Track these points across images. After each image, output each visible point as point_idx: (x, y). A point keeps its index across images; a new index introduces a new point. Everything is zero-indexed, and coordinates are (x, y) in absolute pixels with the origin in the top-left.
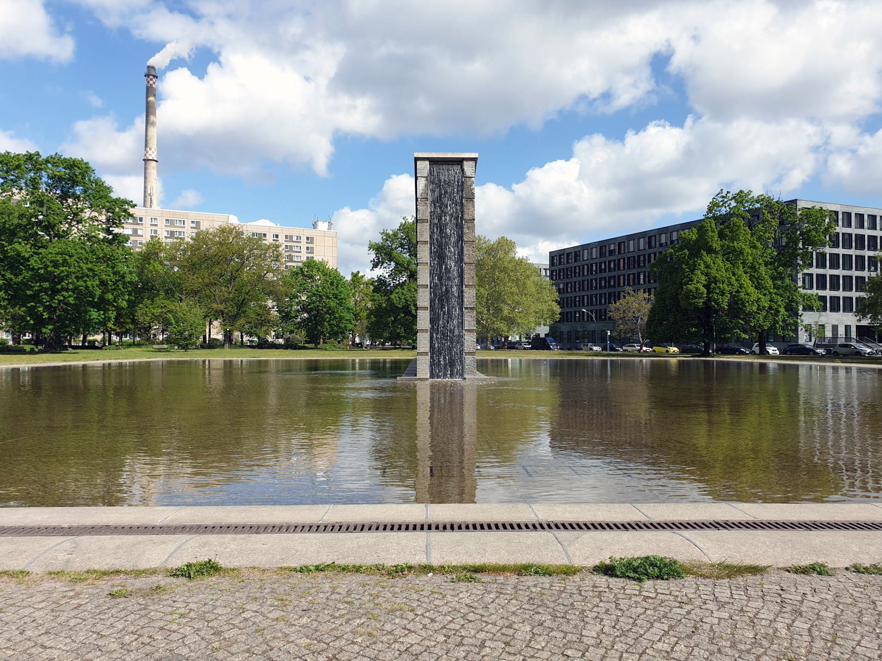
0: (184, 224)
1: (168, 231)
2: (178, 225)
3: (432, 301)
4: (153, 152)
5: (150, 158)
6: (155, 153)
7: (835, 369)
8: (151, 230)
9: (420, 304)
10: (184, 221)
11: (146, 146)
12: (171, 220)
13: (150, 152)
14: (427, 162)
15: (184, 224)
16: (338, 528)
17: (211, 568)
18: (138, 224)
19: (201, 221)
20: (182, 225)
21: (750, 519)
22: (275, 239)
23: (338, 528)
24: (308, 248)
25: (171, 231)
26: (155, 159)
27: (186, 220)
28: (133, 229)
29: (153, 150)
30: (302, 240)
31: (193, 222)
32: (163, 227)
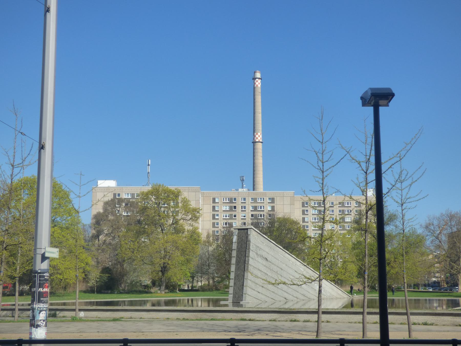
0: (263, 200)
1: (253, 206)
2: (259, 201)
3: (235, 277)
4: (259, 136)
5: (257, 140)
6: (261, 136)
7: (197, 306)
8: (242, 206)
9: (231, 277)
10: (263, 198)
11: (254, 132)
12: (255, 198)
13: (257, 136)
14: (237, 230)
15: (263, 200)
16: (158, 321)
17: (143, 186)
18: (233, 203)
19: (275, 198)
20: (262, 201)
21: (115, 313)
22: (243, 209)
23: (158, 321)
24: (340, 211)
25: (255, 206)
26: (261, 141)
27: (265, 198)
28: (230, 206)
29: (259, 134)
30: (352, 205)
31: (269, 199)
32: (250, 203)
